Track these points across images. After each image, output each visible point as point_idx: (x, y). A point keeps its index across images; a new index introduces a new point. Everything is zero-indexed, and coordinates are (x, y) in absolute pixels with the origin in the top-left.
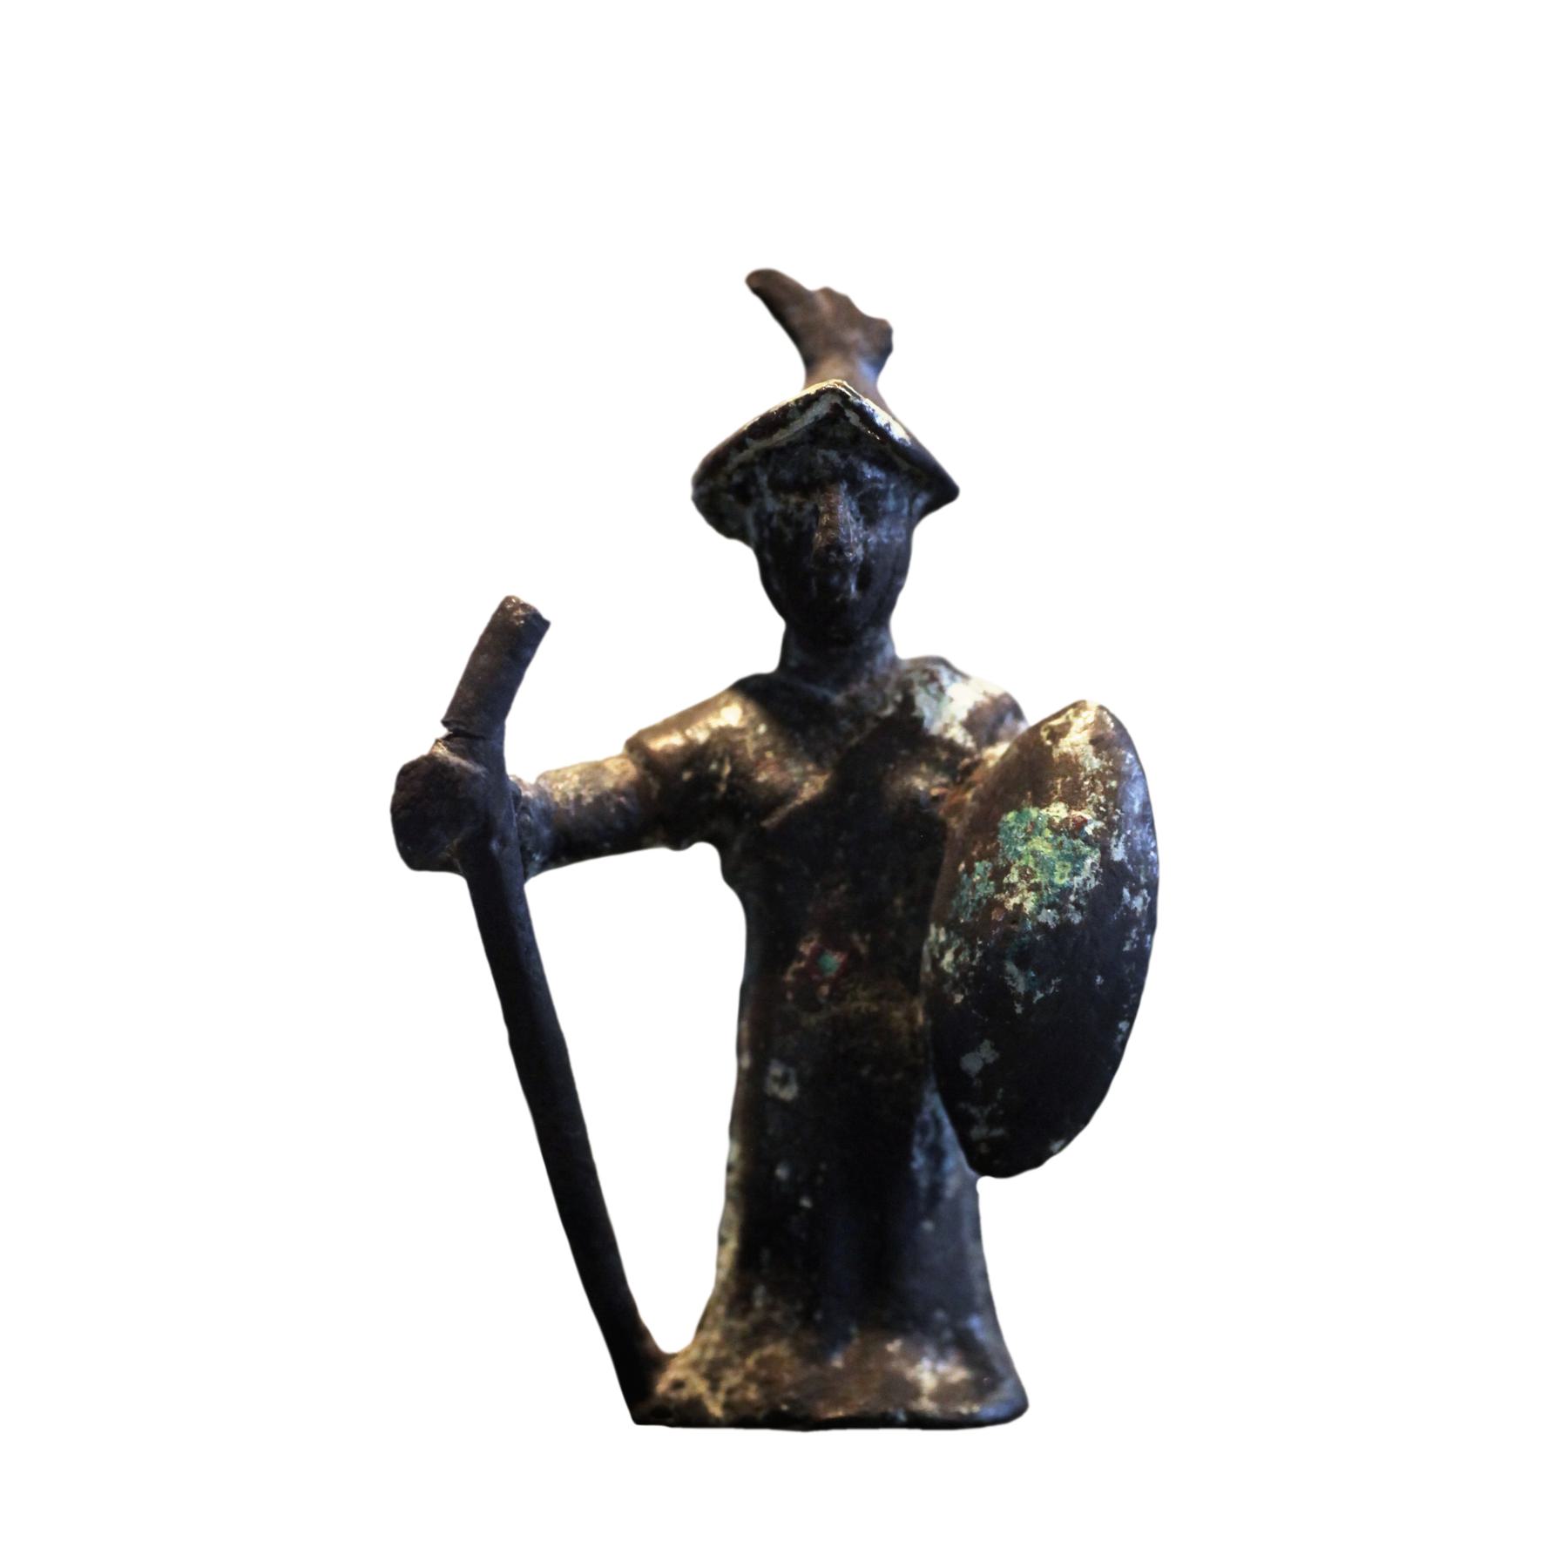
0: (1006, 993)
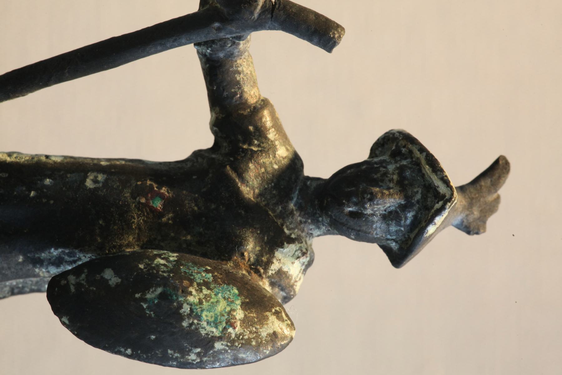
0: (146, 289)
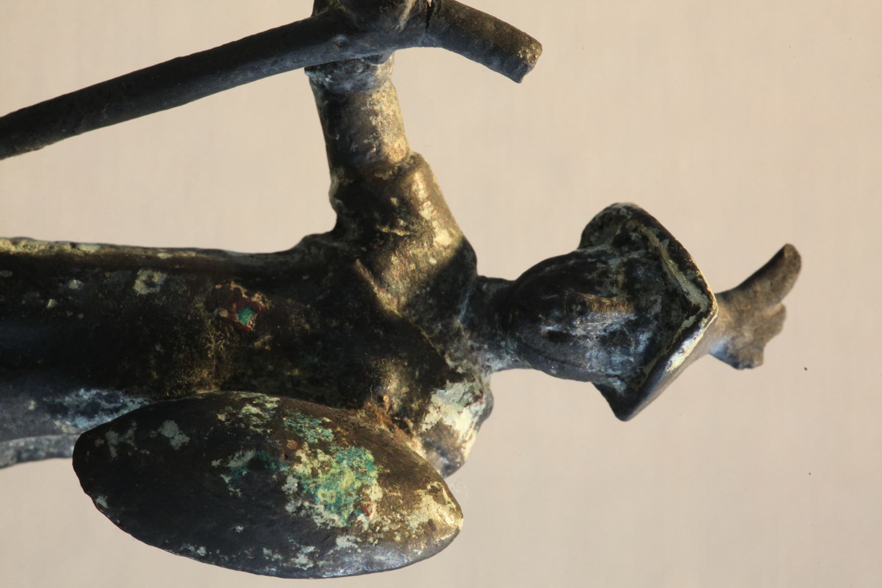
0: (228, 453)
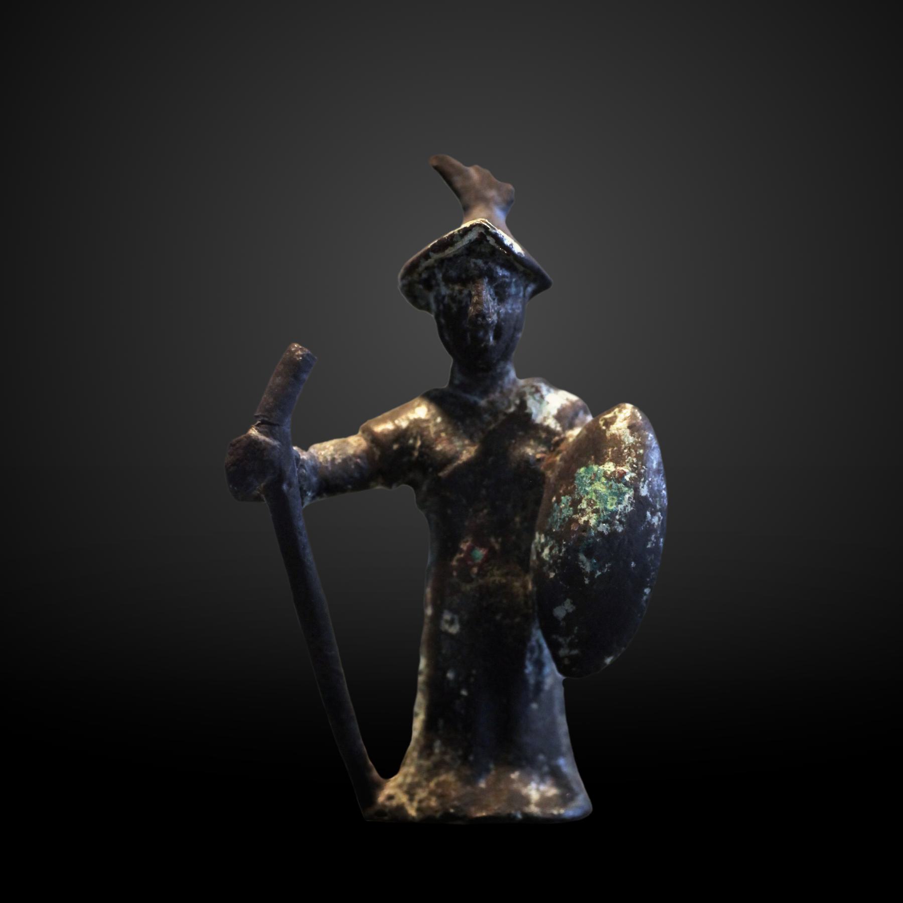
0: (579, 572)
